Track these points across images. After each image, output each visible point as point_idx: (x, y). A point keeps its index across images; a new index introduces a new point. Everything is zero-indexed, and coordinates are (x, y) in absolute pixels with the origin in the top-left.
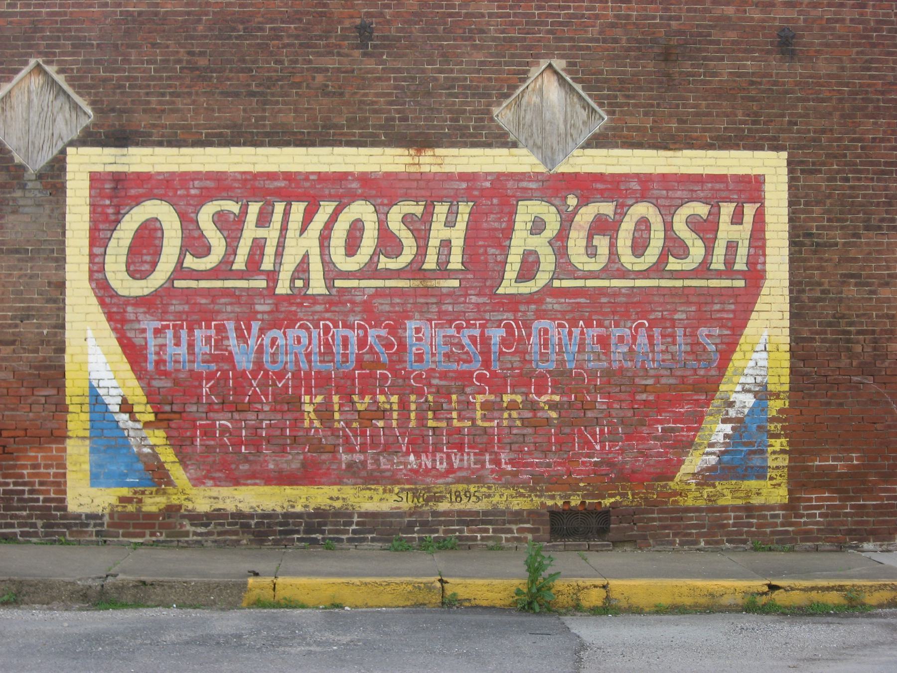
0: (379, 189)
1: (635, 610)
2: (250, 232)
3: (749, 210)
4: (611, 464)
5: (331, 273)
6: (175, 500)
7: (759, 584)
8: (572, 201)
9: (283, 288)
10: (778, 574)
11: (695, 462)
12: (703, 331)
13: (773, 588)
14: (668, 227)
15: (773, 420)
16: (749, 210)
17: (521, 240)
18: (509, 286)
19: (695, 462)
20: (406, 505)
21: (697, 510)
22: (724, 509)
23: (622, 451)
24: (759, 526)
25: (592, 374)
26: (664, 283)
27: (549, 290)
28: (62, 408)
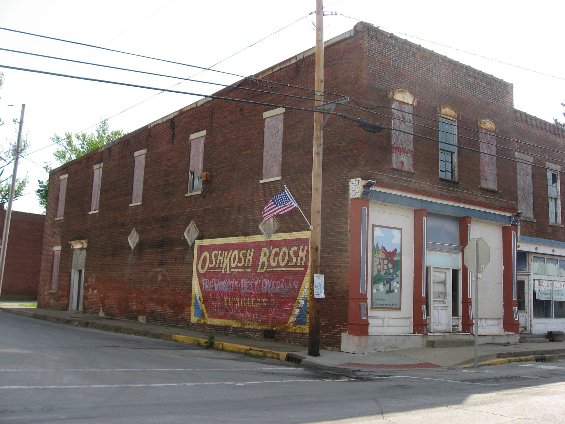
0: (238, 247)
1: (226, 351)
2: (219, 258)
3: (306, 248)
4: (276, 319)
5: (231, 268)
6: (205, 321)
7: (248, 348)
8: (272, 248)
9: (223, 272)
10: (252, 346)
11: (292, 319)
12: (294, 282)
13: (251, 349)
14: (289, 253)
15: (308, 308)
16: (306, 248)
17: (263, 259)
18: (259, 271)
19: (292, 319)
20: (240, 326)
21: (292, 333)
22: (297, 333)
23: (278, 315)
24: (305, 339)
25: (273, 293)
26: (288, 269)
27: (266, 272)
28: (191, 299)
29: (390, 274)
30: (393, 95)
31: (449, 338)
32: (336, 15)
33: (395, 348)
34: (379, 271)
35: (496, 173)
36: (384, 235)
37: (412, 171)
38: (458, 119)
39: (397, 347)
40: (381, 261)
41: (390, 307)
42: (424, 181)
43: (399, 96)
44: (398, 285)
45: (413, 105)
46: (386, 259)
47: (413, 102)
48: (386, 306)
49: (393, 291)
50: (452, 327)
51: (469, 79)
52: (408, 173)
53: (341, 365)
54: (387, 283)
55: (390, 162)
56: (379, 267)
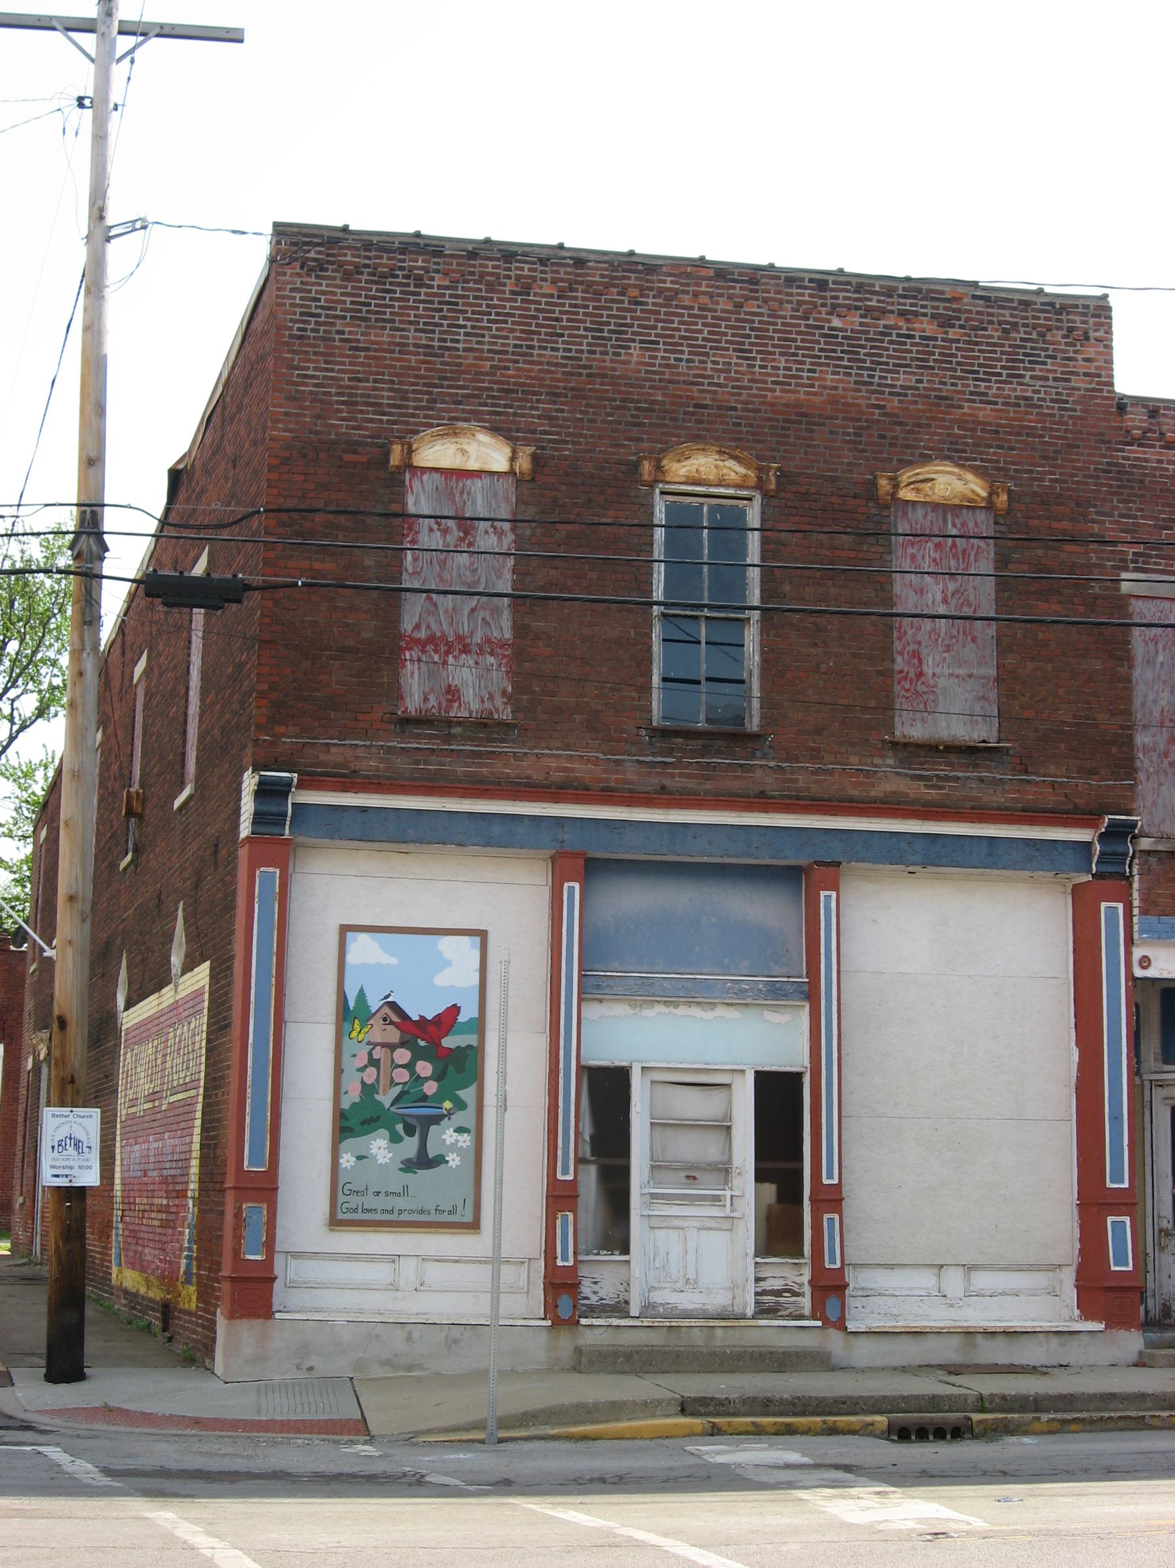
29: (425, 1098)
30: (410, 451)
31: (698, 1338)
32: (144, 228)
33: (410, 1368)
34: (368, 1090)
35: (993, 672)
36: (394, 961)
37: (506, 715)
38: (760, 485)
39: (420, 1367)
40: (378, 1053)
41: (423, 1218)
42: (567, 747)
43: (437, 453)
44: (465, 1140)
45: (512, 472)
46: (403, 1044)
47: (513, 459)
48: (405, 1217)
49: (440, 1160)
50: (751, 1299)
51: (836, 322)
52: (483, 726)
53: (42, 1412)
54: (410, 1131)
55: (396, 692)
56: (370, 1075)
